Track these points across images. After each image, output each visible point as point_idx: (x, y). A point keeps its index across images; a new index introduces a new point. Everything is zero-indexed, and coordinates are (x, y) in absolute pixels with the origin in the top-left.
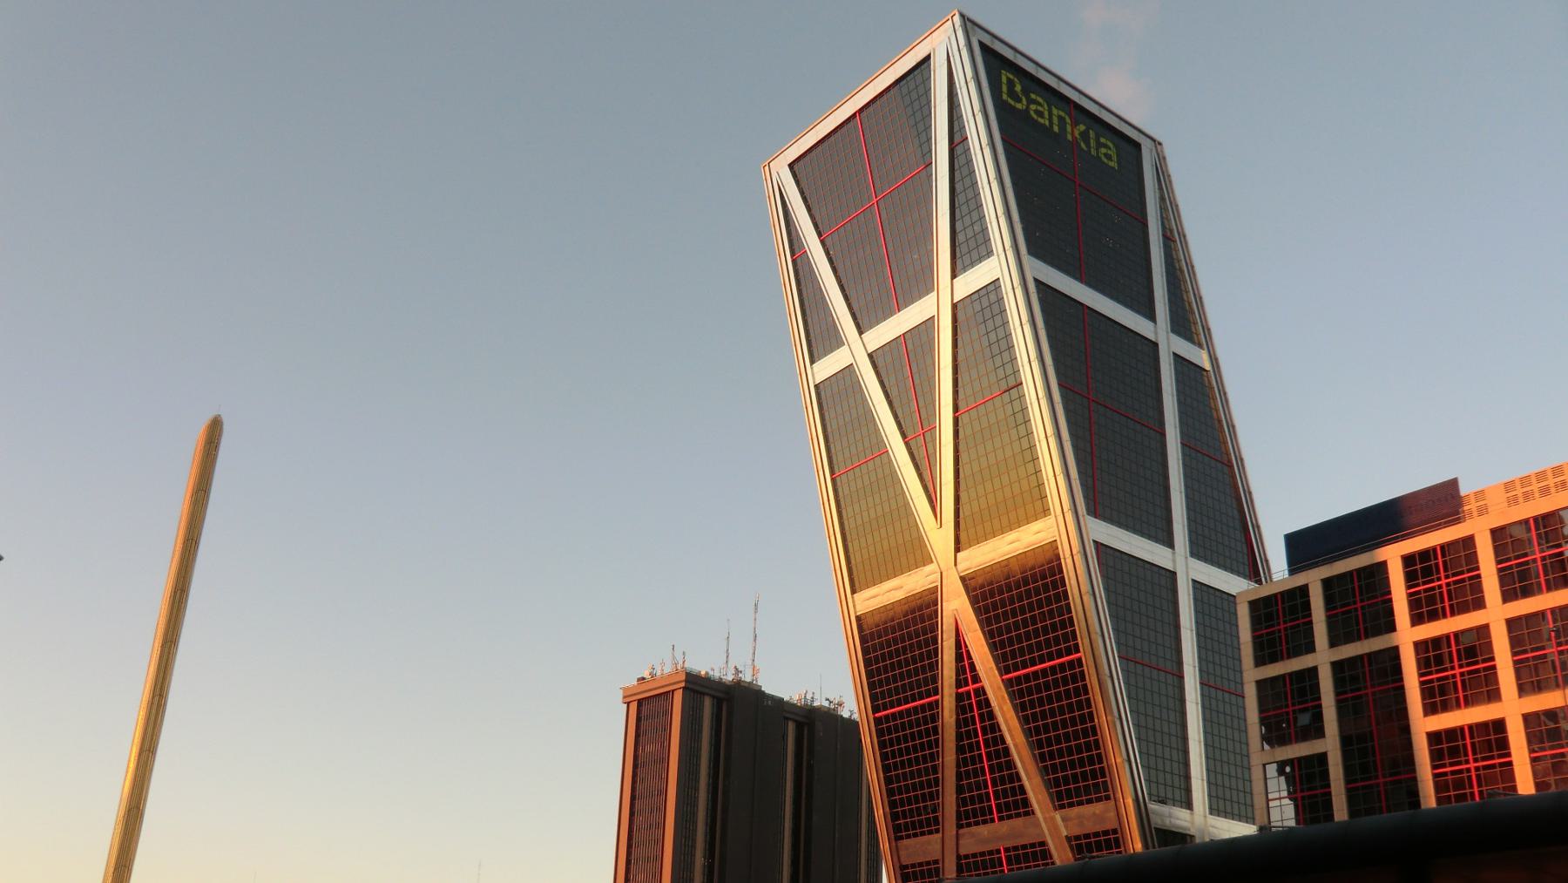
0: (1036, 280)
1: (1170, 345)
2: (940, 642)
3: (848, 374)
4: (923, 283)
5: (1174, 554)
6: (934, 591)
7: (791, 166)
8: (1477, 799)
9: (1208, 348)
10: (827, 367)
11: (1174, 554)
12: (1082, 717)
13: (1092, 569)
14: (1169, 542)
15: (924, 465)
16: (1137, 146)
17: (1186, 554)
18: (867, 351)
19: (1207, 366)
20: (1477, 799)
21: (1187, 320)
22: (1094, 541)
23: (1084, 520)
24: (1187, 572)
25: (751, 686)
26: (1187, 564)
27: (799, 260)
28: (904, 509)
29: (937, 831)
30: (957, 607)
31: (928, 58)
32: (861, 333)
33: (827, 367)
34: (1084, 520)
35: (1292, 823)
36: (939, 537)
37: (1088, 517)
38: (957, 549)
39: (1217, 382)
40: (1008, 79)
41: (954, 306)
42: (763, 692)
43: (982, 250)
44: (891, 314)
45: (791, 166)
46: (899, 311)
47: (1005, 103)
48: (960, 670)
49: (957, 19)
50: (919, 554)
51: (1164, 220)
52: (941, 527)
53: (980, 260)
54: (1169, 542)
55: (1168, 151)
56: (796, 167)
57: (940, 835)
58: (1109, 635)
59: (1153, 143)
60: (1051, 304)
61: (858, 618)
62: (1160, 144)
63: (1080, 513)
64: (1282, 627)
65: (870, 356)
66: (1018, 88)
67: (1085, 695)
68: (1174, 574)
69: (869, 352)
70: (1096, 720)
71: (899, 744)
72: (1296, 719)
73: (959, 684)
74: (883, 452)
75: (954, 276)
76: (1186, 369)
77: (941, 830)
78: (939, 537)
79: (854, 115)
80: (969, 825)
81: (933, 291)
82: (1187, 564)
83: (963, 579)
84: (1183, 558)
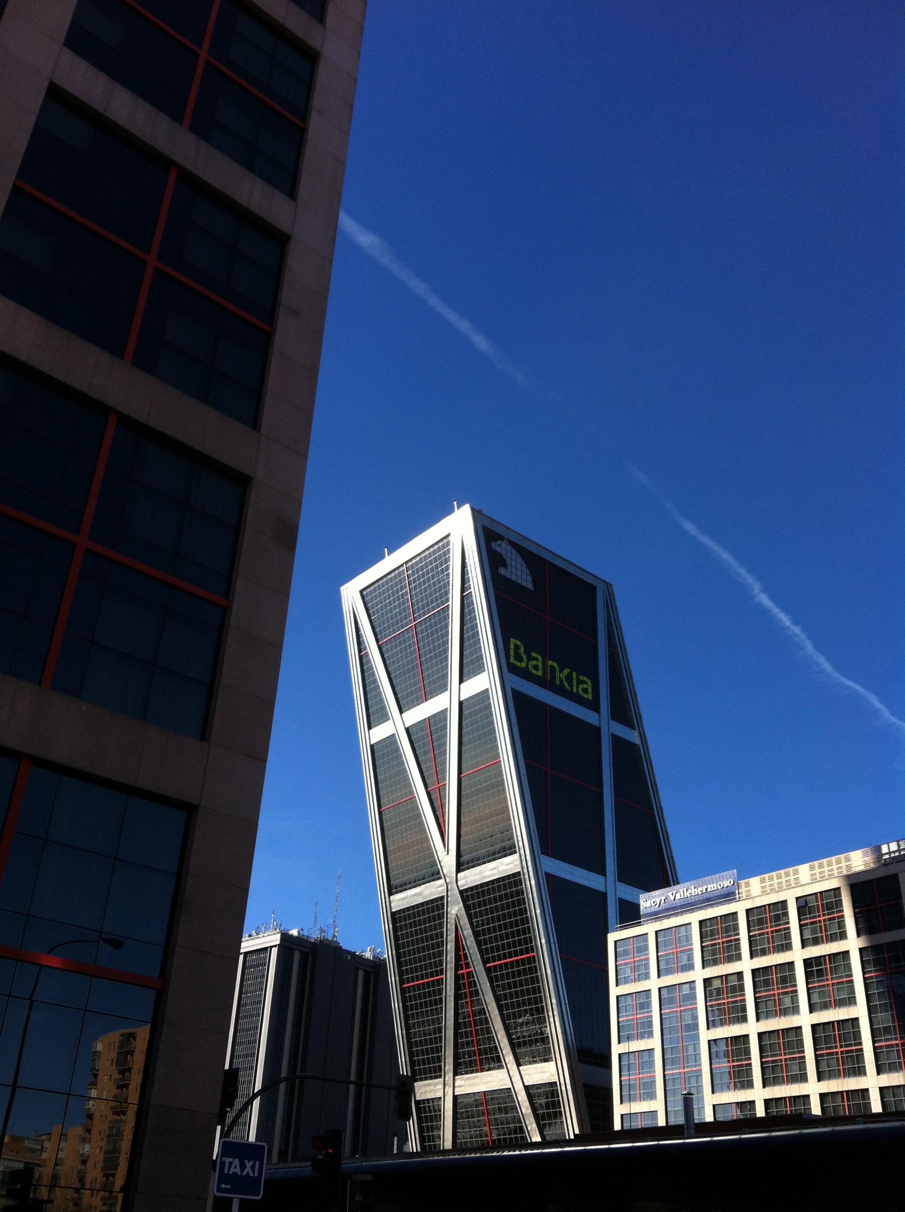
1: (610, 728)
2: (445, 937)
3: (391, 741)
4: (441, 686)
5: (600, 716)
6: (442, 898)
9: (639, 729)
10: (379, 733)
11: (600, 716)
13: (556, 966)
14: (602, 872)
15: (439, 813)
16: (594, 588)
17: (615, 880)
18: (404, 726)
19: (637, 741)
22: (545, 873)
23: (539, 857)
24: (616, 893)
25: (333, 944)
26: (609, 725)
28: (425, 839)
29: (440, 1077)
30: (455, 909)
32: (401, 712)
33: (379, 733)
34: (539, 857)
36: (447, 861)
37: (541, 856)
39: (645, 753)
40: (516, 645)
41: (461, 704)
43: (479, 668)
44: (423, 702)
45: (361, 592)
46: (426, 701)
47: (514, 665)
48: (458, 958)
52: (448, 853)
53: (481, 673)
54: (602, 872)
57: (442, 1079)
58: (561, 980)
59: (605, 584)
62: (611, 585)
63: (536, 852)
65: (407, 730)
66: (522, 650)
67: (522, 895)
68: (604, 895)
69: (407, 726)
70: (529, 913)
73: (456, 970)
75: (461, 681)
76: (620, 745)
77: (443, 1075)
78: (447, 861)
81: (447, 690)
82: (609, 725)
84: (613, 884)
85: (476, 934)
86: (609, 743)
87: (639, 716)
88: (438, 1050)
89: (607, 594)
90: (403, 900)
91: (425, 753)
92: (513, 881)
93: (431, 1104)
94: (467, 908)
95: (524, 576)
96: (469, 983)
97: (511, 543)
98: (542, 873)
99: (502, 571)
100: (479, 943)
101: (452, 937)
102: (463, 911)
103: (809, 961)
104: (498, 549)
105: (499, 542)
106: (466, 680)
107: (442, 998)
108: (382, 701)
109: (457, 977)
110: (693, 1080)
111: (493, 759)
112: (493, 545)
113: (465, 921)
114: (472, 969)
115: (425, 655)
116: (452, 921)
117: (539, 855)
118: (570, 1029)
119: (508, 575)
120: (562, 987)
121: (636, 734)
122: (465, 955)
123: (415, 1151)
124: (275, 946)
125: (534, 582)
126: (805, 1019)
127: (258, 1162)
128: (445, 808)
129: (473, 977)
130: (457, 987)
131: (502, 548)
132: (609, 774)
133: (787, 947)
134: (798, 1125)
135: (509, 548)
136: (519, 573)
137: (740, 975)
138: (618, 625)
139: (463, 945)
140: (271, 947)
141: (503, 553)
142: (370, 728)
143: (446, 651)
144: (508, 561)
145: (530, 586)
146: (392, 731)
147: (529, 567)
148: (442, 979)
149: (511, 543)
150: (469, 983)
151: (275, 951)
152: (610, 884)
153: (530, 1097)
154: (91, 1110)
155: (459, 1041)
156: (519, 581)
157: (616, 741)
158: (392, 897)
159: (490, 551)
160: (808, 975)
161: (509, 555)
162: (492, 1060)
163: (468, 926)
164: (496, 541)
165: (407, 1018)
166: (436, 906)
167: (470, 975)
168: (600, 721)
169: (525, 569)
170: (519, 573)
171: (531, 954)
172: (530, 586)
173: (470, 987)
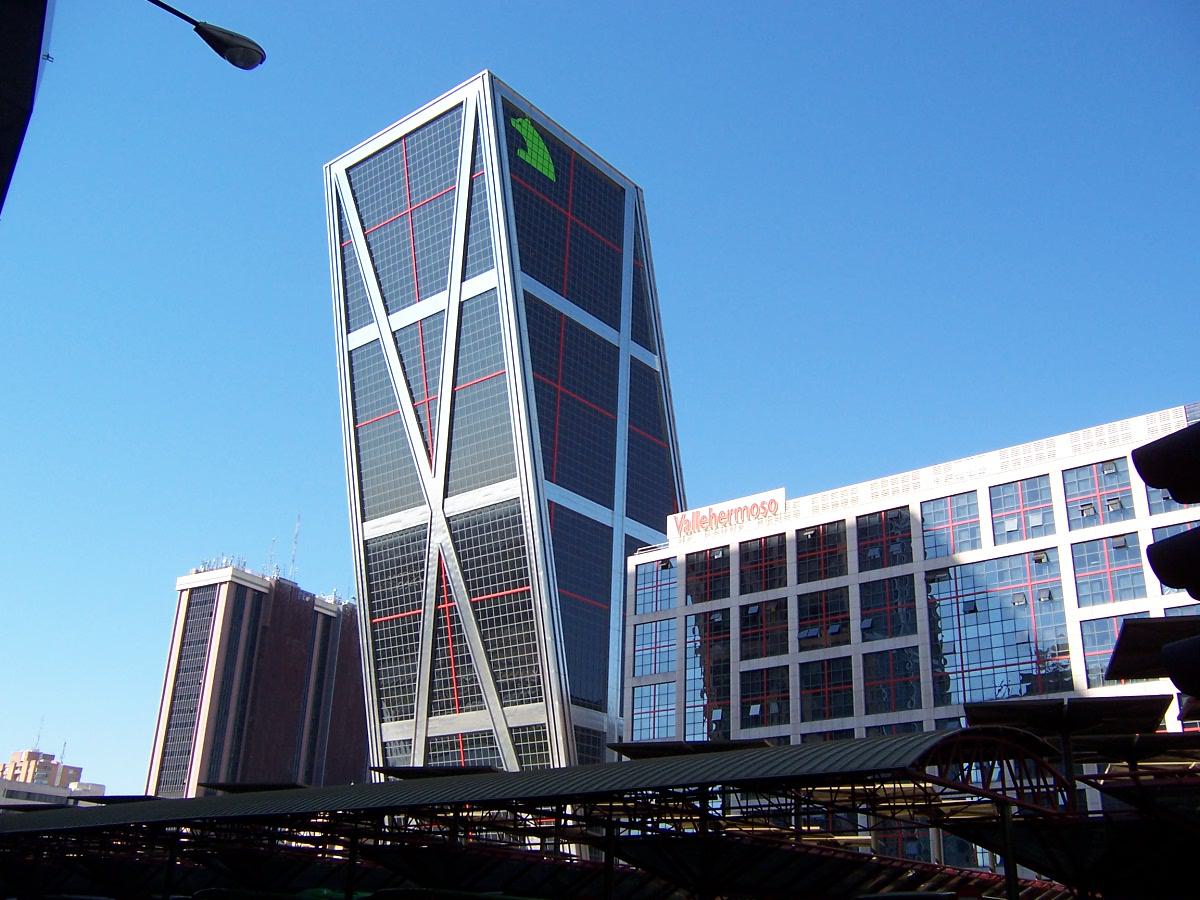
0: (525, 292)
1: (629, 350)
4: (441, 285)
5: (613, 513)
7: (347, 170)
8: (1075, 753)
10: (359, 338)
11: (613, 513)
12: (519, 561)
15: (426, 430)
19: (658, 369)
20: (1075, 753)
21: (645, 332)
27: (346, 249)
30: (440, 538)
31: (461, 105)
33: (359, 338)
35: (607, 761)
36: (433, 485)
38: (445, 496)
41: (461, 304)
42: (299, 589)
43: (488, 265)
45: (347, 170)
49: (486, 77)
50: (417, 498)
51: (637, 234)
53: (488, 270)
55: (646, 197)
56: (351, 173)
60: (535, 315)
61: (366, 543)
62: (641, 190)
64: (708, 575)
71: (447, 702)
72: (888, 547)
73: (437, 603)
74: (392, 399)
76: (639, 370)
79: (400, 139)
80: (436, 714)
81: (446, 289)
83: (448, 520)
84: (620, 518)
85: (463, 567)
87: (661, 341)
88: (411, 689)
90: (376, 528)
91: (415, 371)
92: (512, 509)
93: (393, 717)
94: (454, 537)
95: (546, 164)
96: (452, 619)
97: (533, 123)
99: (521, 153)
100: (465, 576)
101: (433, 569)
102: (449, 540)
103: (838, 591)
104: (518, 127)
105: (520, 120)
106: (469, 278)
107: (418, 634)
108: (365, 300)
109: (437, 613)
111: (497, 369)
112: (513, 122)
113: (450, 552)
114: (456, 603)
115: (421, 238)
116: (434, 557)
119: (528, 160)
121: (657, 358)
122: (449, 588)
123: (378, 781)
124: (226, 582)
125: (557, 172)
126: (856, 649)
128: (434, 425)
129: (456, 612)
130: (437, 622)
131: (523, 127)
133: (726, 594)
135: (531, 128)
136: (540, 160)
137: (726, 612)
139: (446, 577)
140: (221, 583)
141: (524, 133)
142: (348, 332)
143: (448, 243)
144: (529, 144)
145: (552, 176)
146: (376, 335)
147: (552, 153)
148: (420, 614)
149: (533, 123)
150: (452, 619)
151: (224, 589)
153: (515, 739)
155: (436, 680)
156: (539, 168)
157: (635, 363)
158: (383, 724)
159: (510, 131)
160: (1076, 564)
161: (530, 137)
162: (471, 699)
163: (454, 556)
164: (516, 118)
165: (376, 655)
166: (420, 534)
167: (453, 609)
169: (547, 156)
170: (540, 160)
171: (526, 588)
172: (552, 176)
173: (452, 622)
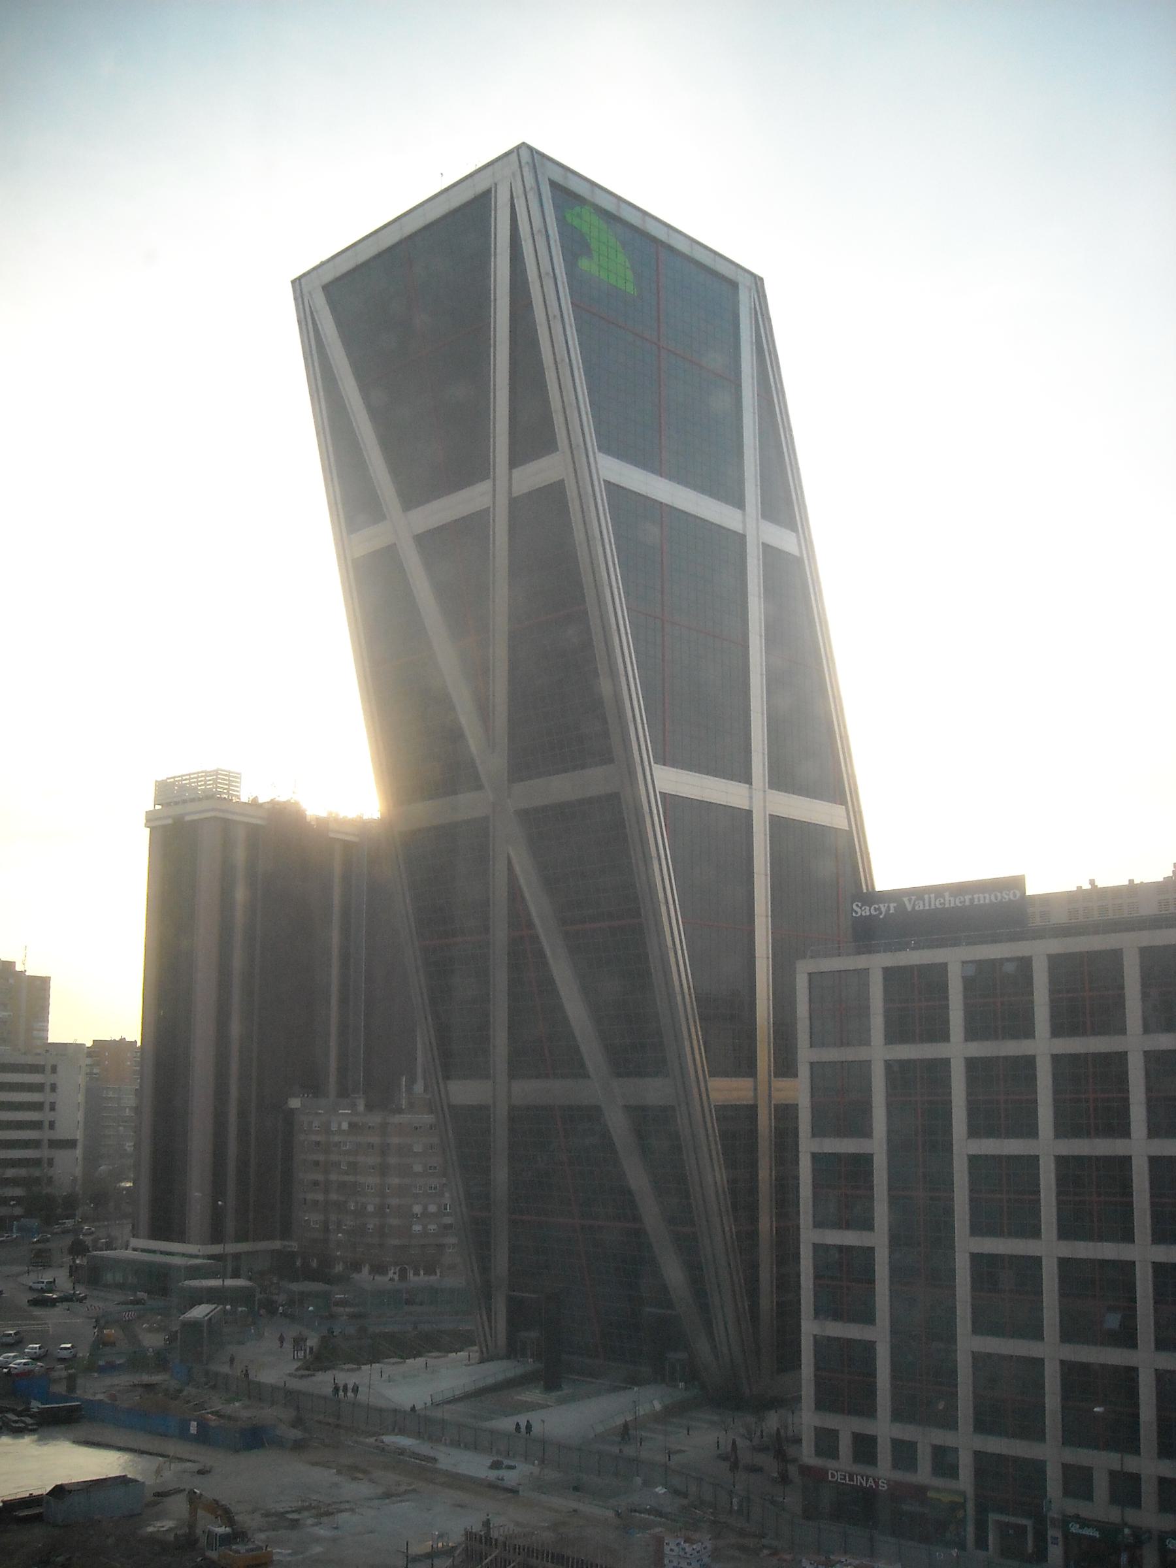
14: (740, 504)
16: (734, 285)
54: (740, 504)
68: (749, 813)
76: (771, 554)
86: (753, 387)
89: (756, 296)
98: (599, 483)
104: (576, 222)
105: (578, 209)
110: (890, 1062)
112: (568, 217)
117: (594, 453)
118: (657, 806)
120: (617, 579)
127: (192, 1432)
132: (762, 836)
134: (1164, 916)
138: (772, 350)
144: (594, 245)
152: (758, 796)
154: (1078, 1526)
168: (744, 522)
